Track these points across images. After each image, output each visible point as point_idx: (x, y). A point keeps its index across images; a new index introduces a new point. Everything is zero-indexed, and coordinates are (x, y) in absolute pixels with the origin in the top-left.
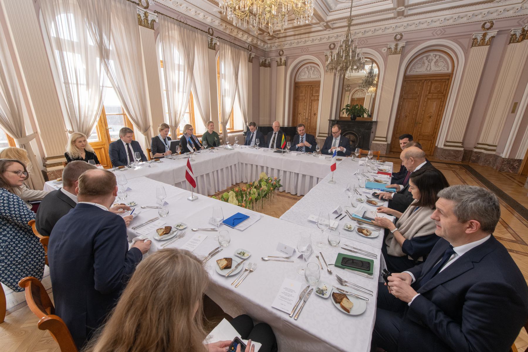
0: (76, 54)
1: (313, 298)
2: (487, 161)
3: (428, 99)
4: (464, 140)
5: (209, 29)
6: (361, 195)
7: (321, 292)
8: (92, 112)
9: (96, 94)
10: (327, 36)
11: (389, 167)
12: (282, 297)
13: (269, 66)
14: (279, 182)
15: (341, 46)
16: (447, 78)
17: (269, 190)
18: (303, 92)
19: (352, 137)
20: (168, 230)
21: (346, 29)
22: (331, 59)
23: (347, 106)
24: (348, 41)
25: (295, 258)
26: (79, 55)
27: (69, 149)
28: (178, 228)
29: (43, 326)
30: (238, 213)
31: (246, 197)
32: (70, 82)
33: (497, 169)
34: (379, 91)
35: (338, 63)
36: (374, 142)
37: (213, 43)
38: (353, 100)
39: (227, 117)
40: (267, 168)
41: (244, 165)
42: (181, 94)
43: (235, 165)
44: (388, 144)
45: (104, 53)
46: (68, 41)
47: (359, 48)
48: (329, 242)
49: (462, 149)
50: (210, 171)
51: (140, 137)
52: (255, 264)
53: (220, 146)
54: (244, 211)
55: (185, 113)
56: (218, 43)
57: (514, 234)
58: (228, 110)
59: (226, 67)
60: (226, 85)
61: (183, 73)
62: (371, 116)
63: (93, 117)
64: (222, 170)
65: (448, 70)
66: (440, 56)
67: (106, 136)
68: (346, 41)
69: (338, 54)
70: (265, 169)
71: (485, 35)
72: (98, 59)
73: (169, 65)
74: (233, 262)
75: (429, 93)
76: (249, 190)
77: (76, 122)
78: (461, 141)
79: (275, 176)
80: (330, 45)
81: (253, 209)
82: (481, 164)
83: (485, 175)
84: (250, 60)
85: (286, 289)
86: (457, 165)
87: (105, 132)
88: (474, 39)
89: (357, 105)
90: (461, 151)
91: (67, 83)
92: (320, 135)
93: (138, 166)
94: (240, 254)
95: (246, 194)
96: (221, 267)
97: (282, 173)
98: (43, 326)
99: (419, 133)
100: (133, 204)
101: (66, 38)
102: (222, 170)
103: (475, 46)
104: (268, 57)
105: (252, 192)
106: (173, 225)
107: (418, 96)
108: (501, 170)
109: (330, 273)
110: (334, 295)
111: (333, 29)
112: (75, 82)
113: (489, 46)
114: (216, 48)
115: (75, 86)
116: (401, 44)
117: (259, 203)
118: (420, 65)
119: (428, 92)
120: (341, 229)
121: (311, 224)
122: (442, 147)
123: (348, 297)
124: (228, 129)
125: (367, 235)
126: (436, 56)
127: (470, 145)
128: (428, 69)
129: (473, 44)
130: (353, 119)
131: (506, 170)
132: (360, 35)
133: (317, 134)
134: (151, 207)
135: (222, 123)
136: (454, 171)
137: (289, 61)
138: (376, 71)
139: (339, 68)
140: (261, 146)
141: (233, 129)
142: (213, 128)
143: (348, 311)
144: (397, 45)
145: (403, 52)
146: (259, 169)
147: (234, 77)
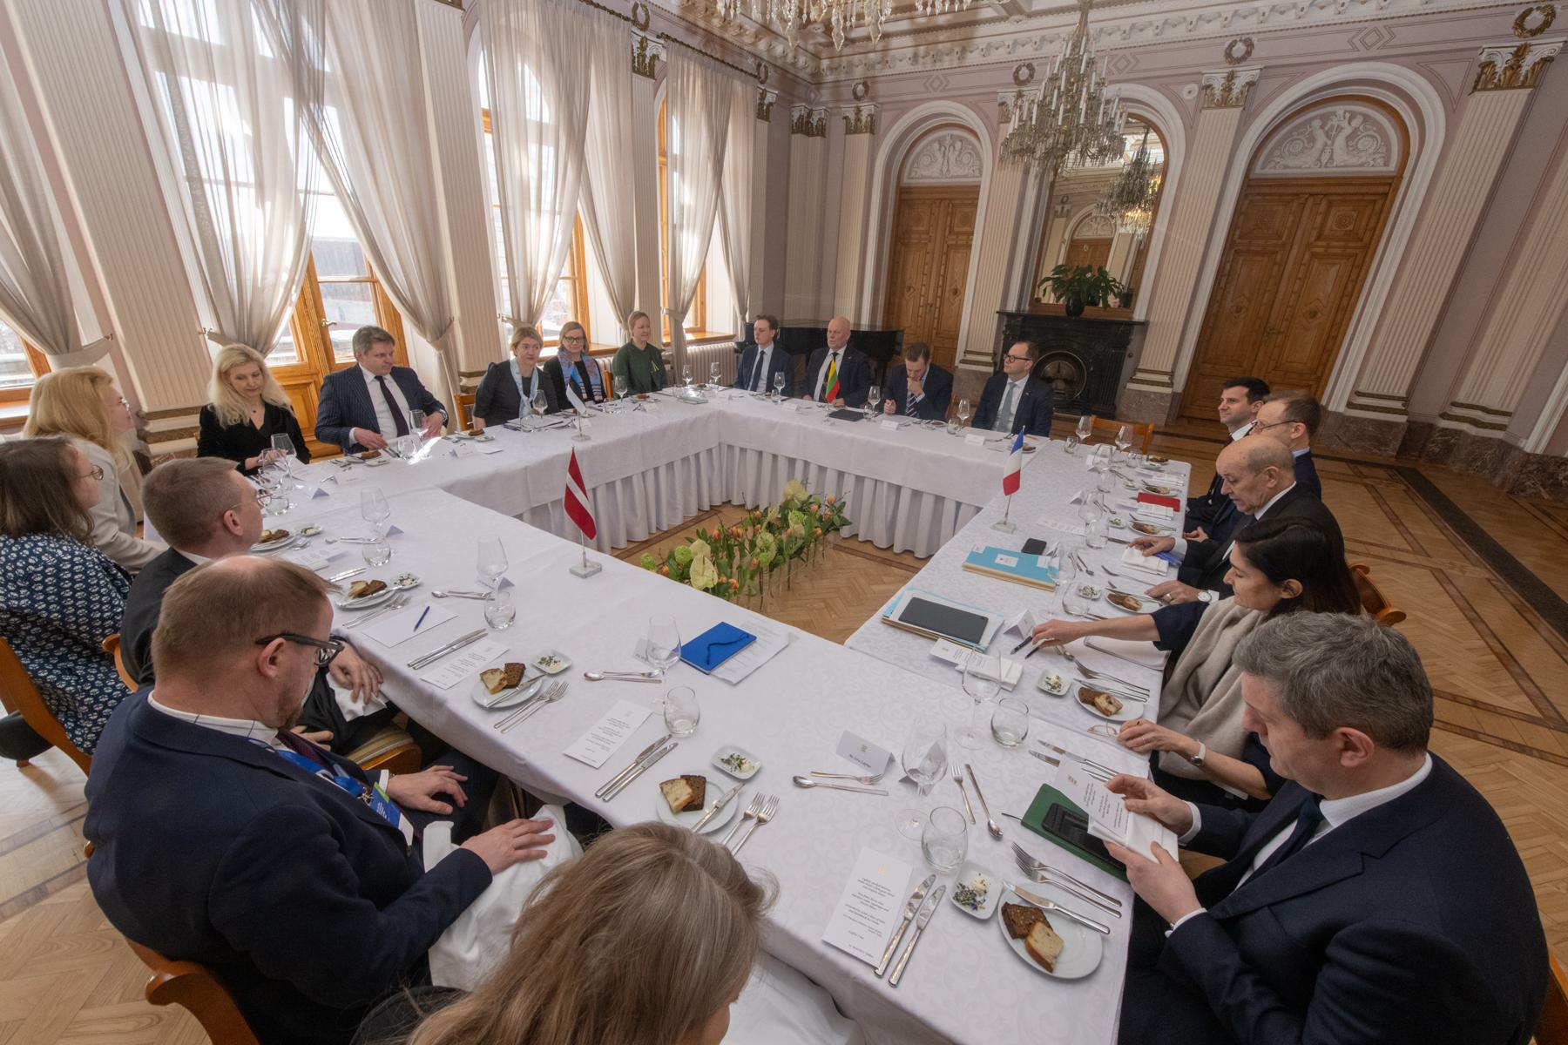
0: (221, 87)
1: (945, 919)
2: (1475, 460)
3: (1313, 255)
4: (1410, 391)
5: (636, 6)
6: (1091, 573)
7: (967, 899)
8: (277, 273)
9: (284, 220)
10: (1009, 40)
11: (1176, 478)
12: (853, 909)
13: (821, 131)
14: (840, 510)
15: (1054, 79)
16: (1381, 190)
17: (811, 534)
18: (925, 220)
19: (1066, 368)
20: (513, 675)
21: (1075, 17)
22: (1020, 120)
23: (1058, 270)
24: (1079, 61)
25: (891, 782)
26: (231, 89)
27: (213, 394)
28: (543, 667)
29: (158, 995)
30: (723, 624)
31: (742, 556)
32: (204, 175)
33: (1502, 485)
34: (1161, 228)
35: (1040, 131)
36: (1131, 386)
37: (648, 53)
38: (1074, 245)
39: (685, 294)
40: (807, 464)
41: (737, 451)
42: (546, 218)
43: (710, 451)
44: (1174, 394)
45: (307, 87)
46: (192, 40)
47: (1111, 82)
48: (994, 731)
49: (1402, 419)
50: (634, 470)
51: (423, 357)
52: (774, 801)
53: (666, 390)
54: (739, 617)
55: (558, 278)
56: (663, 56)
57: (1539, 697)
58: (689, 270)
59: (684, 137)
60: (684, 193)
61: (552, 150)
62: (1128, 298)
63: (281, 291)
64: (670, 466)
65: (1386, 164)
66: (1366, 118)
67: (322, 349)
68: (1072, 62)
69: (1043, 106)
70: (799, 466)
71: (1520, 53)
72: (289, 104)
73: (509, 127)
74: (709, 788)
75: (1318, 238)
76: (750, 534)
77: (228, 305)
78: (1402, 393)
79: (830, 493)
80: (1017, 71)
81: (761, 609)
82: (1456, 468)
83: (1464, 502)
84: (763, 113)
85: (865, 882)
86: (1381, 466)
87: (319, 335)
88: (1484, 66)
89: (1089, 269)
90: (1397, 425)
91: (195, 179)
92: (969, 357)
93: (423, 450)
94: (728, 762)
95: (741, 546)
96: (674, 805)
97: (849, 484)
98: (158, 995)
99: (1272, 364)
100: (408, 584)
101: (186, 34)
102: (670, 466)
103: (1485, 89)
104: (819, 104)
105: (759, 543)
106: (527, 657)
107: (1284, 245)
108: (1515, 490)
109: (996, 835)
110: (1007, 910)
111: (1030, 16)
112: (221, 177)
113: (1524, 93)
114: (657, 69)
115: (222, 188)
116: (1244, 75)
117: (781, 574)
118: (1298, 146)
119: (1315, 233)
120: (1029, 688)
121: (940, 667)
122: (1342, 409)
123: (1050, 918)
124: (689, 331)
125: (1106, 712)
126: (1353, 115)
127: (1428, 407)
128: (1325, 158)
129: (1477, 82)
130: (1075, 310)
131: (1529, 491)
132: (1116, 40)
133: (960, 355)
134: (462, 595)
135: (670, 312)
136: (1370, 488)
137: (885, 118)
138: (1156, 154)
139: (1040, 150)
140: (789, 393)
141: (702, 329)
142: (648, 335)
143: (1049, 967)
144: (1231, 77)
145: (1248, 100)
146: (783, 466)
147: (710, 167)
